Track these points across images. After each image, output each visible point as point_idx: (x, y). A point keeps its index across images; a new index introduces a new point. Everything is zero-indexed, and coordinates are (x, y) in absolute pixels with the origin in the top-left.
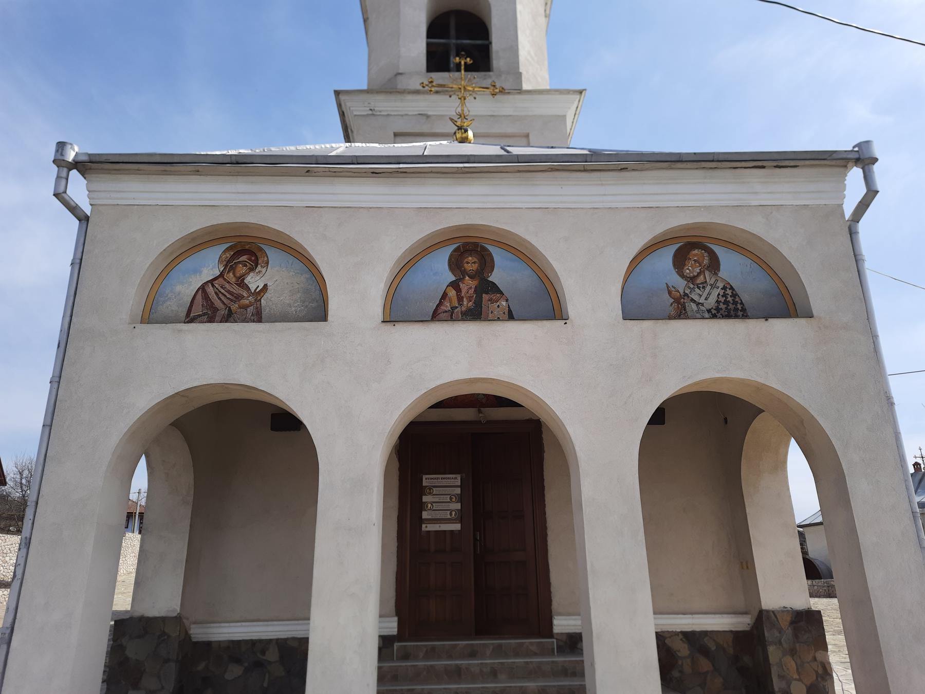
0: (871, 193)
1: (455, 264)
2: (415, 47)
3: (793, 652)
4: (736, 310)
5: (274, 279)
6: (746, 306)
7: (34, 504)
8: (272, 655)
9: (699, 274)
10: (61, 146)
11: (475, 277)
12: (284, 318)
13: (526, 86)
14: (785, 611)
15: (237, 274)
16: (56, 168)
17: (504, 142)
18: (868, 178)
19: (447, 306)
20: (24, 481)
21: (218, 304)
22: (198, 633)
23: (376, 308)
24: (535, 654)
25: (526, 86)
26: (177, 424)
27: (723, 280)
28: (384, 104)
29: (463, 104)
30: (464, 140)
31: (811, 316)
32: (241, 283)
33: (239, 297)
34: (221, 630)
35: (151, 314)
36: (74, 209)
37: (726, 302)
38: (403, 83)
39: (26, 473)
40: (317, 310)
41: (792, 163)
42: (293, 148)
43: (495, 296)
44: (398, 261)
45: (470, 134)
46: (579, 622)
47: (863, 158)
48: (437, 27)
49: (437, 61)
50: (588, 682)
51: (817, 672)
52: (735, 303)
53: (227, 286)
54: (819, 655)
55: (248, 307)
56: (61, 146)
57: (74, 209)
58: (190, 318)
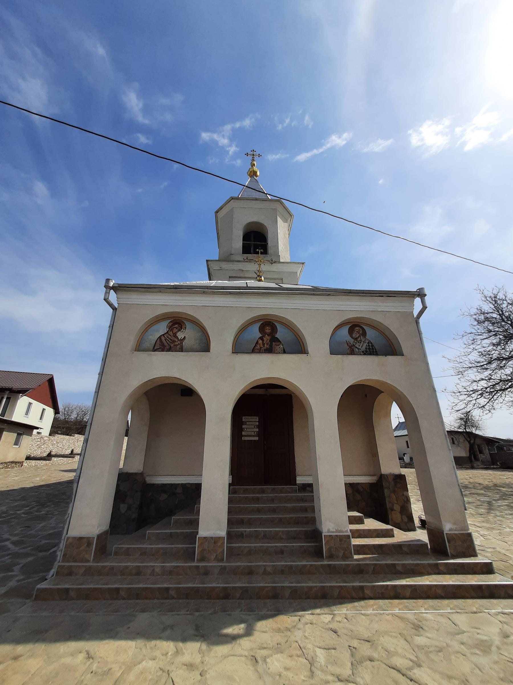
0: (424, 308)
1: (262, 329)
2: (238, 244)
3: (394, 492)
4: (373, 351)
5: (187, 334)
6: (377, 350)
7: (90, 425)
8: (179, 490)
9: (358, 337)
10: (108, 281)
11: (270, 336)
12: (191, 350)
13: (281, 261)
14: (391, 475)
15: (175, 333)
16: (105, 289)
17: (277, 281)
18: (423, 302)
19: (258, 347)
20: (66, 412)
21: (166, 344)
22: (150, 480)
23: (229, 346)
24: (289, 492)
25: (281, 261)
26: (146, 394)
27: (368, 340)
28: (225, 266)
29: (260, 267)
30: (260, 280)
31: (402, 355)
32: (175, 336)
33: (174, 341)
34: (158, 479)
35: (139, 348)
36: (111, 305)
37: (369, 349)
38: (234, 258)
39: (67, 409)
40: (205, 347)
41: (393, 295)
42: (195, 282)
43: (277, 343)
44: (239, 328)
45: (263, 278)
46: (312, 479)
47: (421, 294)
48: (247, 237)
49: (246, 250)
50: (316, 504)
51: (404, 500)
52: (373, 349)
53: (169, 337)
54: (405, 493)
55: (178, 345)
56: (108, 281)
57: (111, 305)
58: (154, 350)
